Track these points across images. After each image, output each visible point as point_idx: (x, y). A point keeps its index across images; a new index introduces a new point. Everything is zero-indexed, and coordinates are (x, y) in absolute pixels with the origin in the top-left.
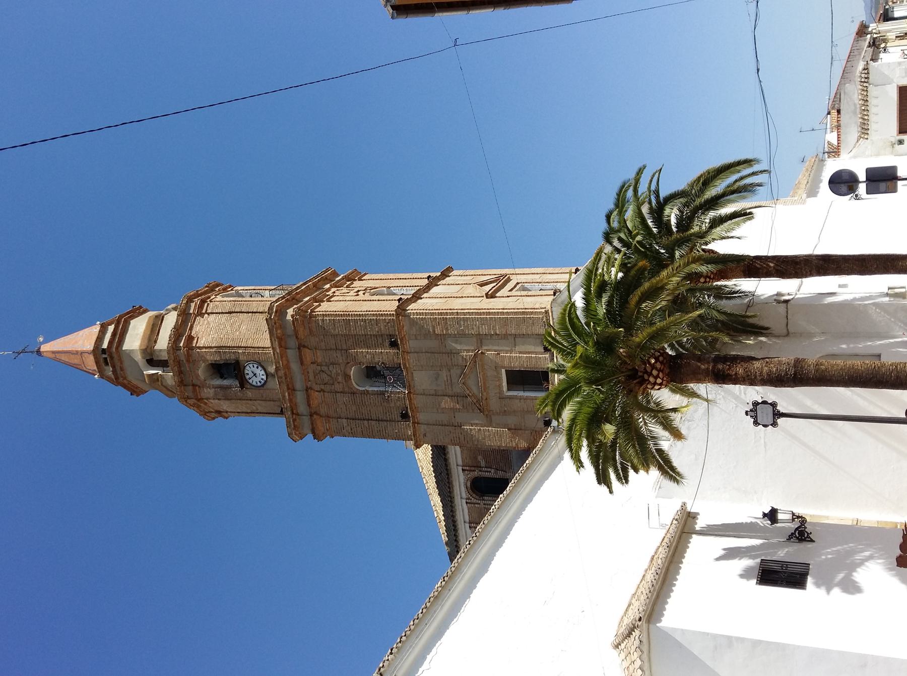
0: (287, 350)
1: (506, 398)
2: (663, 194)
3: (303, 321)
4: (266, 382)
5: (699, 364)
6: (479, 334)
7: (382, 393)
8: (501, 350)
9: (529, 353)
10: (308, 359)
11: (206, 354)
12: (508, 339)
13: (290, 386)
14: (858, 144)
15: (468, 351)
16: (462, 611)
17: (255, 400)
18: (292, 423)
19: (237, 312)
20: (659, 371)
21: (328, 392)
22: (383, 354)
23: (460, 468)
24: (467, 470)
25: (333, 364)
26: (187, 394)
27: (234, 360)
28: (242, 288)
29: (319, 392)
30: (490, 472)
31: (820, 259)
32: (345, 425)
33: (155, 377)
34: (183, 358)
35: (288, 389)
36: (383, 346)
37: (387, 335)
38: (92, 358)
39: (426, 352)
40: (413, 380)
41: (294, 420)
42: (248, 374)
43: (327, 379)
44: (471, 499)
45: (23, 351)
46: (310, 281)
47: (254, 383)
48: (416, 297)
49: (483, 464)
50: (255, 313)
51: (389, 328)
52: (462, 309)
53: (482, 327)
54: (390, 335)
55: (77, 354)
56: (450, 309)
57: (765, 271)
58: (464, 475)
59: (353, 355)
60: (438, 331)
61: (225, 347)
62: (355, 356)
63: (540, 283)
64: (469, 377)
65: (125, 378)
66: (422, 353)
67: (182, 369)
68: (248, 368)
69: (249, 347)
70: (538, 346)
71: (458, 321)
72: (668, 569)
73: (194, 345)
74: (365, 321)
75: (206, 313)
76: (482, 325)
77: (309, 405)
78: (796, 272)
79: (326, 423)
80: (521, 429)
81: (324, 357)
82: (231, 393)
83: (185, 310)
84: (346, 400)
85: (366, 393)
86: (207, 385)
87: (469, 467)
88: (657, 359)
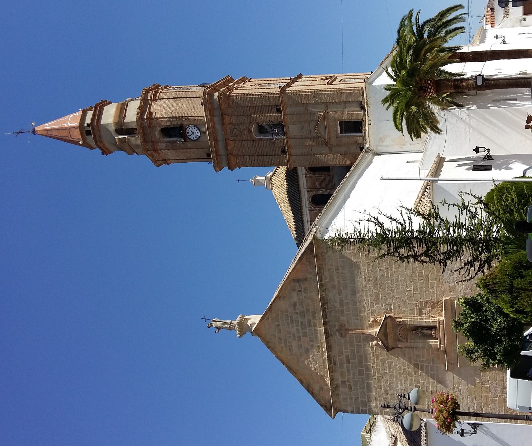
0: (214, 117)
1: (339, 137)
2: (421, 22)
3: (225, 99)
4: (199, 137)
5: (448, 83)
6: (326, 102)
7: (271, 139)
8: (338, 111)
9: (352, 111)
10: (227, 122)
11: (162, 122)
12: (341, 104)
13: (215, 138)
14: (503, 20)
15: (320, 112)
16: (343, 208)
17: (192, 149)
18: (216, 160)
19: (179, 98)
20: (432, 86)
21: (238, 141)
22: (273, 117)
23: (306, 190)
24: (310, 191)
25: (242, 124)
26: (147, 147)
27: (180, 124)
28: (176, 87)
29: (233, 141)
30: (323, 191)
31: (491, 52)
32: (247, 159)
33: (123, 140)
34: (146, 125)
35: (214, 140)
36: (272, 112)
37: (274, 105)
38: (78, 131)
39: (296, 114)
40: (289, 130)
41: (217, 159)
42: (188, 133)
43: (238, 133)
44: (312, 208)
45: (21, 132)
46: (221, 81)
47: (192, 138)
48: (289, 85)
49: (318, 186)
50: (191, 98)
51: (275, 101)
52: (317, 89)
53: (328, 98)
54: (276, 105)
55: (66, 129)
56: (310, 90)
57: (468, 58)
58: (308, 194)
59: (254, 118)
60: (304, 102)
61: (174, 117)
62: (255, 119)
63: (354, 79)
64: (320, 127)
65: (101, 142)
66: (294, 114)
67: (145, 132)
68: (188, 129)
69: (190, 117)
70: (357, 108)
71: (315, 95)
72: (436, 171)
73: (153, 117)
74: (262, 98)
75: (159, 99)
76: (328, 97)
77: (227, 149)
78: (481, 59)
79: (236, 159)
80: (347, 154)
81: (236, 120)
82: (177, 145)
83: (145, 97)
84: (249, 145)
85: (261, 140)
86: (161, 141)
87: (311, 189)
88: (431, 82)
